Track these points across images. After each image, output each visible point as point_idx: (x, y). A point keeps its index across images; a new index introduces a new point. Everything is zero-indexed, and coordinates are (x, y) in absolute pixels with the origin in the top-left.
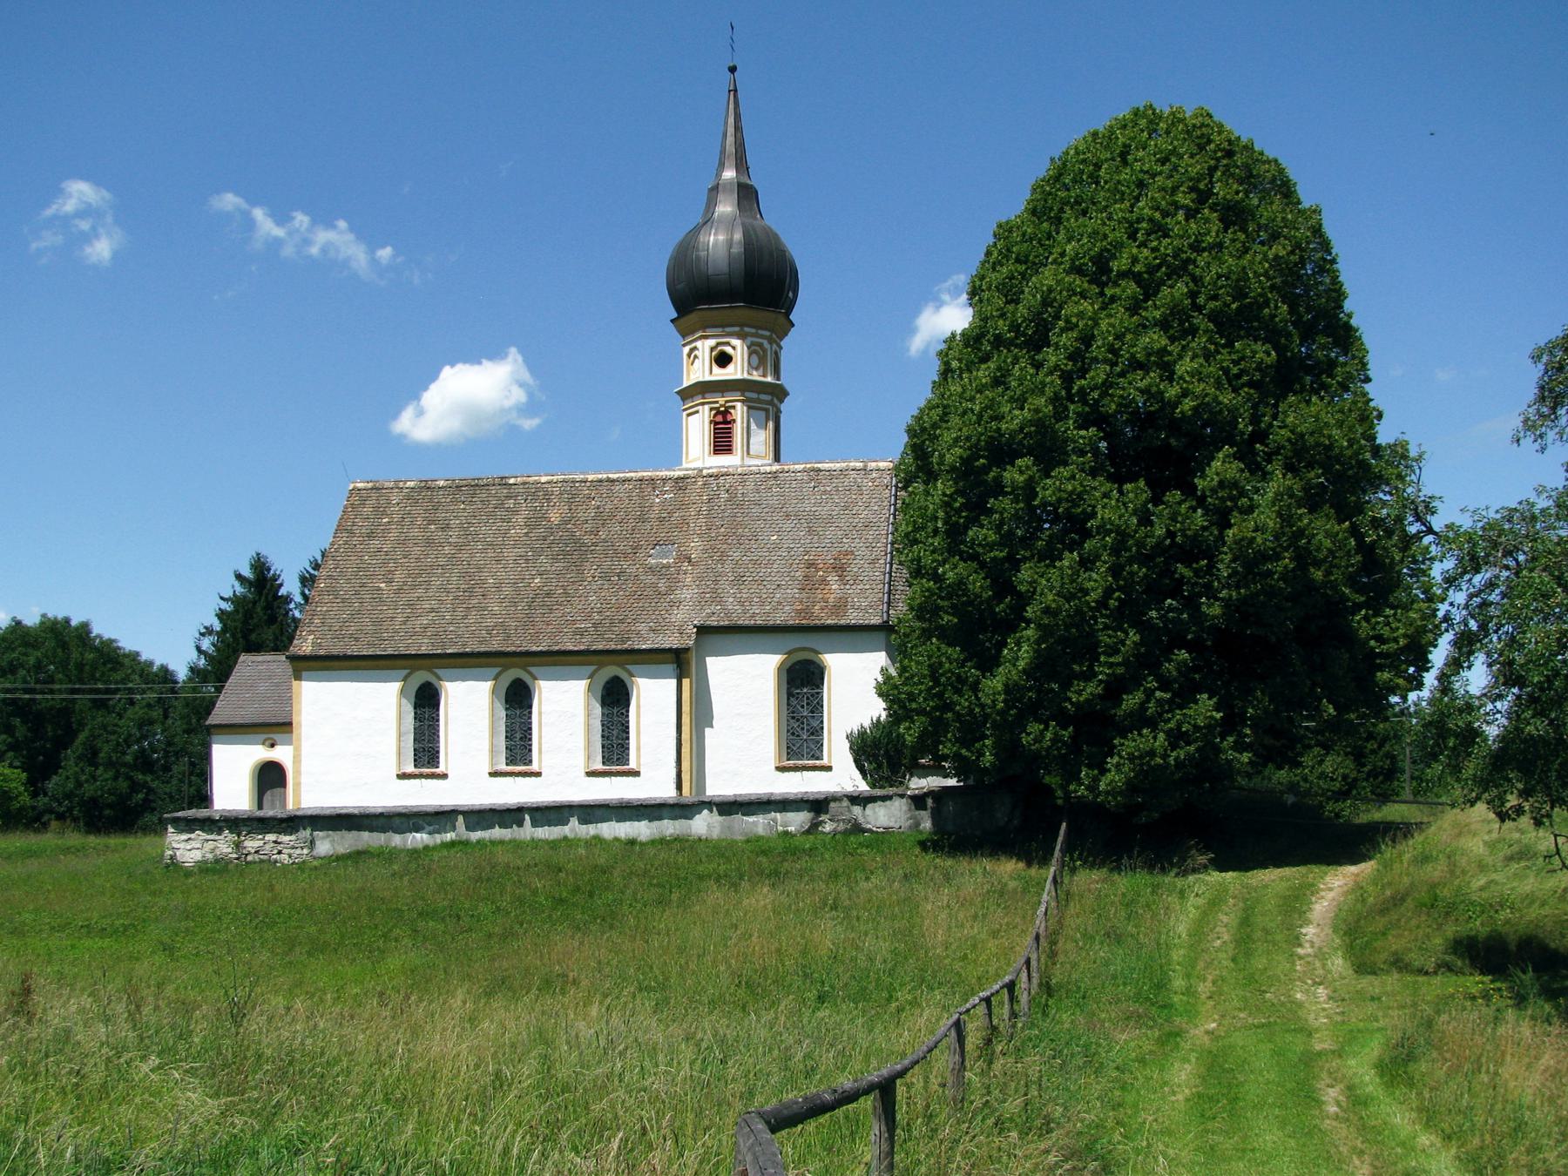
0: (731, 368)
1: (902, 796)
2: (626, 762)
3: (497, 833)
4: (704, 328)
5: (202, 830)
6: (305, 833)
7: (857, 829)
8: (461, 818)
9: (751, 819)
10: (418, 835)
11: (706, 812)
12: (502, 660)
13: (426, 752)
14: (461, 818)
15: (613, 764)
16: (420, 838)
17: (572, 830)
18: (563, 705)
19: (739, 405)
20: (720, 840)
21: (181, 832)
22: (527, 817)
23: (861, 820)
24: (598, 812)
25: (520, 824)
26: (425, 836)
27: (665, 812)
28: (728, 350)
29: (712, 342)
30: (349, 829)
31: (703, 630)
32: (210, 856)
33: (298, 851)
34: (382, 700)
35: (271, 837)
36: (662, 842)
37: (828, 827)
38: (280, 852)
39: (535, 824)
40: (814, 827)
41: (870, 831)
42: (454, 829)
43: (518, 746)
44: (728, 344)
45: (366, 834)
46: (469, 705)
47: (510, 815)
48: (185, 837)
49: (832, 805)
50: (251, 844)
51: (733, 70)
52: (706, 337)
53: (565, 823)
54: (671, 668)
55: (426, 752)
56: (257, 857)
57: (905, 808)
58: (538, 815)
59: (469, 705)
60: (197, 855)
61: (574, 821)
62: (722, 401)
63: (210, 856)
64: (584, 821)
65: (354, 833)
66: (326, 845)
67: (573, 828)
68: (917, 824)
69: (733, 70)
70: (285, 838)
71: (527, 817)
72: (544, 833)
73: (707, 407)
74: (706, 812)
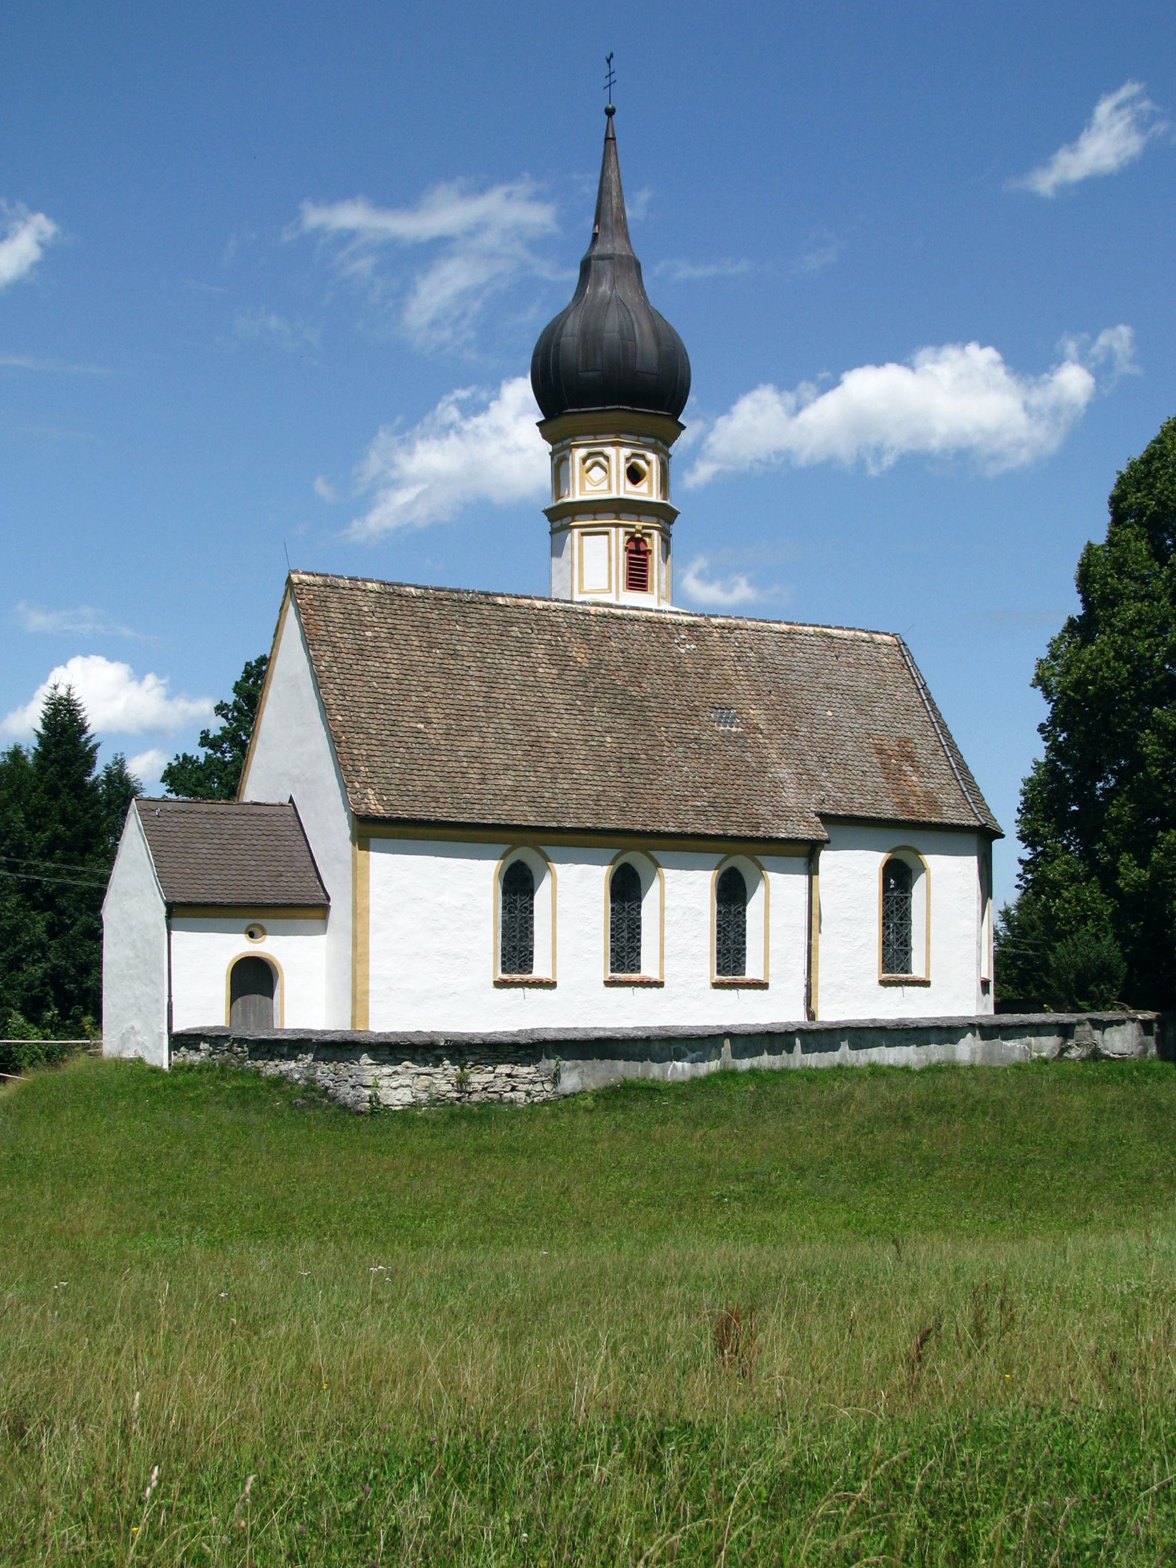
0: (643, 487)
1: (1134, 1020)
2: (638, 968)
3: (766, 1061)
4: (618, 433)
5: (413, 1061)
6: (549, 1064)
7: (1096, 1055)
8: (727, 1042)
9: (1009, 1044)
10: (679, 1064)
11: (969, 1035)
12: (513, 835)
13: (516, 951)
14: (727, 1042)
15: (621, 971)
16: (680, 1069)
17: (843, 1056)
18: (681, 899)
19: (655, 533)
20: (982, 1067)
21: (383, 1063)
22: (798, 1041)
23: (1100, 1045)
24: (870, 1036)
25: (790, 1049)
26: (687, 1065)
27: (933, 1035)
28: (642, 463)
29: (626, 452)
30: (602, 1057)
31: (826, 819)
32: (424, 1096)
33: (538, 1087)
34: (477, 879)
35: (504, 1069)
36: (934, 1070)
37: (1073, 1053)
38: (513, 1089)
39: (806, 1049)
40: (1064, 1049)
41: (1107, 1057)
42: (719, 1056)
43: (624, 949)
44: (643, 457)
45: (621, 1064)
46: (574, 893)
47: (863, 1035)
48: (387, 1070)
49: (1078, 1029)
50: (479, 1078)
51: (610, 113)
52: (622, 445)
53: (835, 1048)
54: (801, 861)
55: (516, 951)
56: (484, 1095)
57: (1136, 1033)
58: (810, 1039)
59: (574, 893)
60: (406, 1096)
61: (845, 1046)
62: (639, 525)
63: (424, 1096)
64: (855, 1046)
65: (608, 1062)
66: (574, 1077)
67: (845, 1055)
68: (1145, 1051)
69: (610, 113)
70: (522, 1070)
71: (798, 1041)
72: (814, 1060)
73: (621, 530)
74: (969, 1035)
